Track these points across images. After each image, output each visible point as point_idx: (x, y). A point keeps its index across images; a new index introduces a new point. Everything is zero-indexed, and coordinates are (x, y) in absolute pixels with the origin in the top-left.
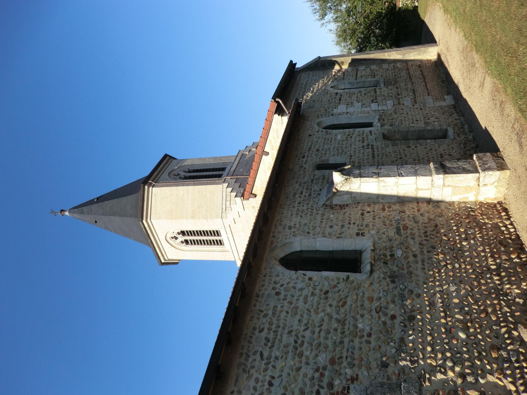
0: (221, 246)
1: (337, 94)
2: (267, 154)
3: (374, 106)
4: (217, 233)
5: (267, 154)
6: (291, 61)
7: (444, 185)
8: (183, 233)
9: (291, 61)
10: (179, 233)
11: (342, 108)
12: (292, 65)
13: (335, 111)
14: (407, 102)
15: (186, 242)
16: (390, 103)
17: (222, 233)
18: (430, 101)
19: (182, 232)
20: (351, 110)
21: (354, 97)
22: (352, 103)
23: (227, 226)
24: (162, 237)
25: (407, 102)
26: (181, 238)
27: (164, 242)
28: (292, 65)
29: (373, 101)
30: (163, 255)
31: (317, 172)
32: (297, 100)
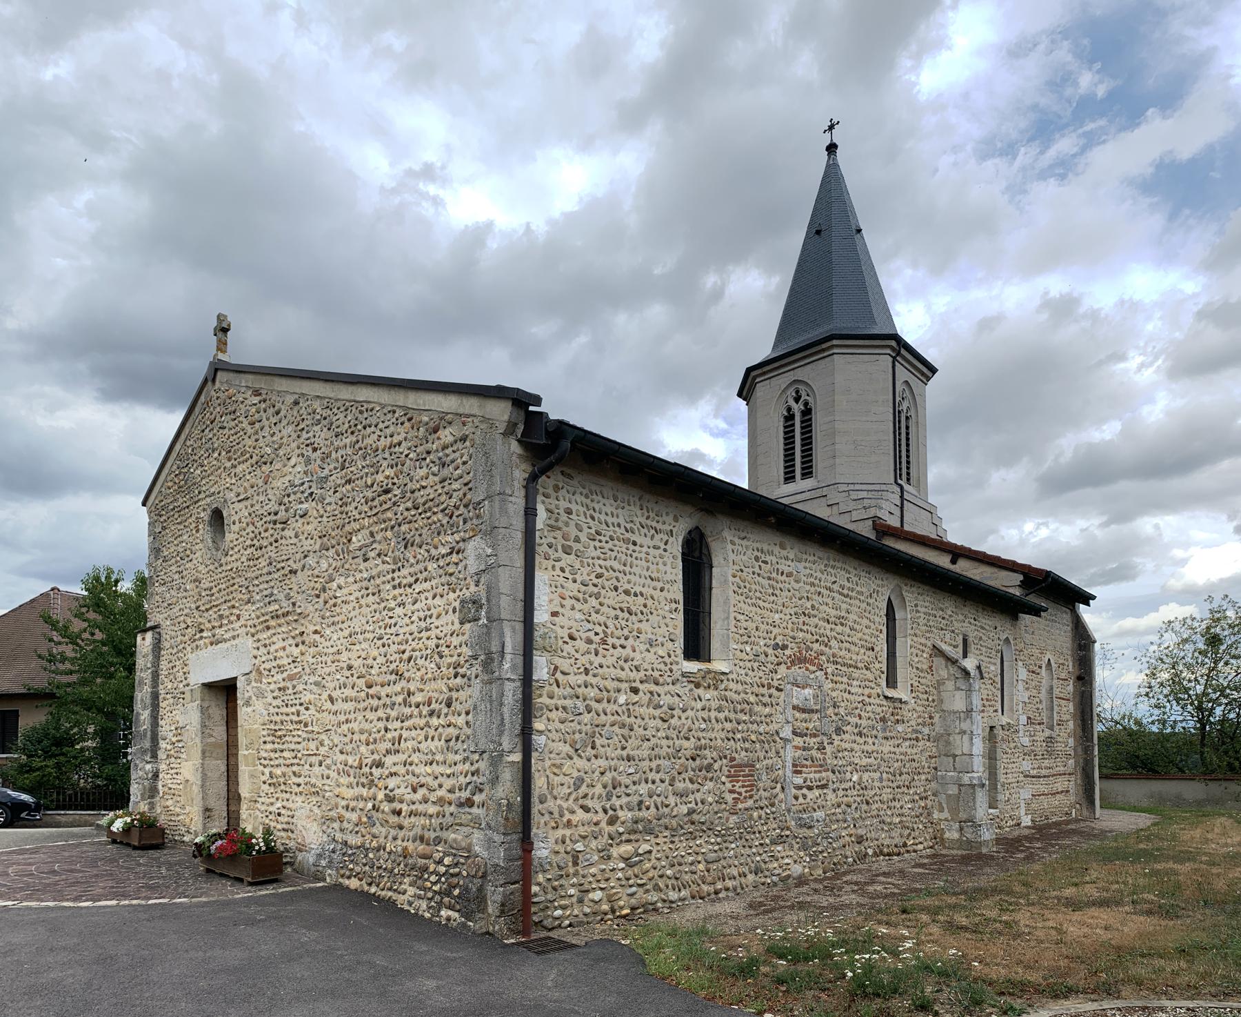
0: (782, 479)
1: (1040, 667)
2: (954, 562)
3: (1023, 719)
4: (807, 473)
5: (954, 562)
6: (1094, 598)
7: (960, 785)
8: (807, 412)
9: (1094, 598)
10: (806, 404)
11: (1023, 674)
12: (1086, 599)
13: (1020, 663)
14: (1026, 765)
15: (790, 417)
16: (1026, 741)
17: (809, 483)
18: (1026, 794)
19: (810, 410)
20: (1021, 686)
21: (1034, 692)
22: (1027, 689)
23: (825, 491)
24: (800, 374)
25: (1026, 765)
26: (797, 408)
27: (790, 377)
28: (1086, 599)
29: (1029, 718)
30: (764, 373)
31: (961, 637)
32: (1046, 610)
